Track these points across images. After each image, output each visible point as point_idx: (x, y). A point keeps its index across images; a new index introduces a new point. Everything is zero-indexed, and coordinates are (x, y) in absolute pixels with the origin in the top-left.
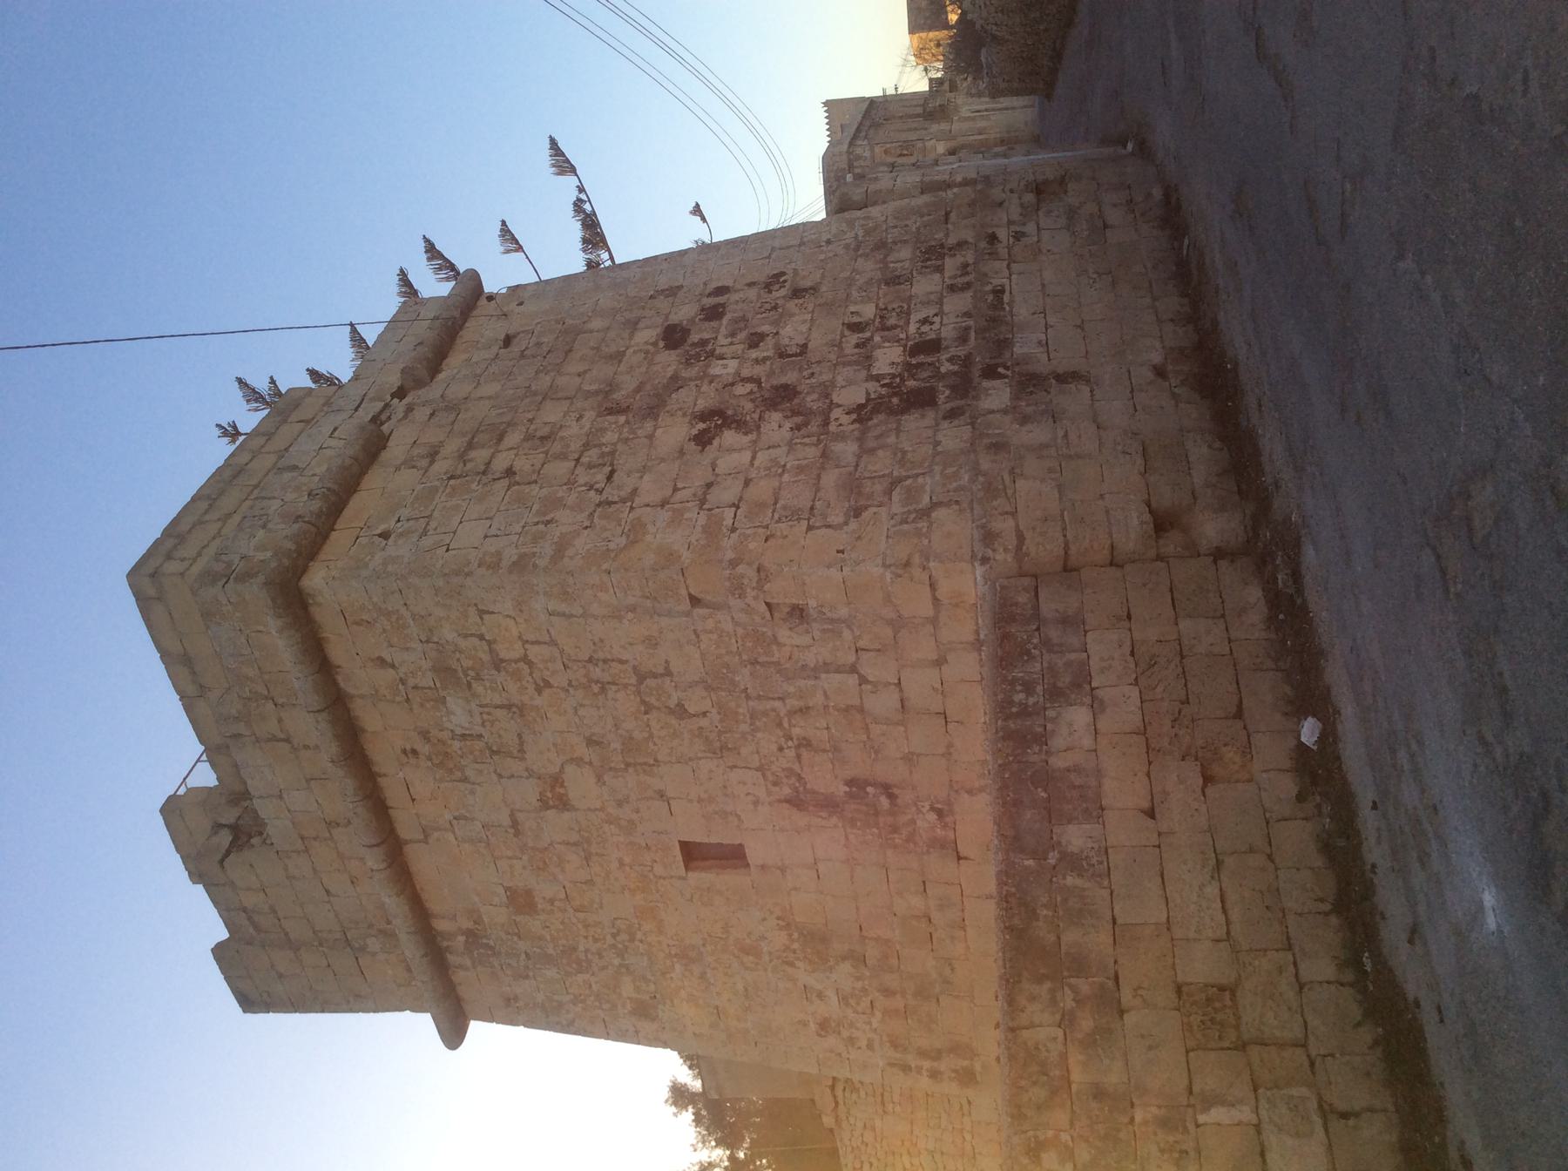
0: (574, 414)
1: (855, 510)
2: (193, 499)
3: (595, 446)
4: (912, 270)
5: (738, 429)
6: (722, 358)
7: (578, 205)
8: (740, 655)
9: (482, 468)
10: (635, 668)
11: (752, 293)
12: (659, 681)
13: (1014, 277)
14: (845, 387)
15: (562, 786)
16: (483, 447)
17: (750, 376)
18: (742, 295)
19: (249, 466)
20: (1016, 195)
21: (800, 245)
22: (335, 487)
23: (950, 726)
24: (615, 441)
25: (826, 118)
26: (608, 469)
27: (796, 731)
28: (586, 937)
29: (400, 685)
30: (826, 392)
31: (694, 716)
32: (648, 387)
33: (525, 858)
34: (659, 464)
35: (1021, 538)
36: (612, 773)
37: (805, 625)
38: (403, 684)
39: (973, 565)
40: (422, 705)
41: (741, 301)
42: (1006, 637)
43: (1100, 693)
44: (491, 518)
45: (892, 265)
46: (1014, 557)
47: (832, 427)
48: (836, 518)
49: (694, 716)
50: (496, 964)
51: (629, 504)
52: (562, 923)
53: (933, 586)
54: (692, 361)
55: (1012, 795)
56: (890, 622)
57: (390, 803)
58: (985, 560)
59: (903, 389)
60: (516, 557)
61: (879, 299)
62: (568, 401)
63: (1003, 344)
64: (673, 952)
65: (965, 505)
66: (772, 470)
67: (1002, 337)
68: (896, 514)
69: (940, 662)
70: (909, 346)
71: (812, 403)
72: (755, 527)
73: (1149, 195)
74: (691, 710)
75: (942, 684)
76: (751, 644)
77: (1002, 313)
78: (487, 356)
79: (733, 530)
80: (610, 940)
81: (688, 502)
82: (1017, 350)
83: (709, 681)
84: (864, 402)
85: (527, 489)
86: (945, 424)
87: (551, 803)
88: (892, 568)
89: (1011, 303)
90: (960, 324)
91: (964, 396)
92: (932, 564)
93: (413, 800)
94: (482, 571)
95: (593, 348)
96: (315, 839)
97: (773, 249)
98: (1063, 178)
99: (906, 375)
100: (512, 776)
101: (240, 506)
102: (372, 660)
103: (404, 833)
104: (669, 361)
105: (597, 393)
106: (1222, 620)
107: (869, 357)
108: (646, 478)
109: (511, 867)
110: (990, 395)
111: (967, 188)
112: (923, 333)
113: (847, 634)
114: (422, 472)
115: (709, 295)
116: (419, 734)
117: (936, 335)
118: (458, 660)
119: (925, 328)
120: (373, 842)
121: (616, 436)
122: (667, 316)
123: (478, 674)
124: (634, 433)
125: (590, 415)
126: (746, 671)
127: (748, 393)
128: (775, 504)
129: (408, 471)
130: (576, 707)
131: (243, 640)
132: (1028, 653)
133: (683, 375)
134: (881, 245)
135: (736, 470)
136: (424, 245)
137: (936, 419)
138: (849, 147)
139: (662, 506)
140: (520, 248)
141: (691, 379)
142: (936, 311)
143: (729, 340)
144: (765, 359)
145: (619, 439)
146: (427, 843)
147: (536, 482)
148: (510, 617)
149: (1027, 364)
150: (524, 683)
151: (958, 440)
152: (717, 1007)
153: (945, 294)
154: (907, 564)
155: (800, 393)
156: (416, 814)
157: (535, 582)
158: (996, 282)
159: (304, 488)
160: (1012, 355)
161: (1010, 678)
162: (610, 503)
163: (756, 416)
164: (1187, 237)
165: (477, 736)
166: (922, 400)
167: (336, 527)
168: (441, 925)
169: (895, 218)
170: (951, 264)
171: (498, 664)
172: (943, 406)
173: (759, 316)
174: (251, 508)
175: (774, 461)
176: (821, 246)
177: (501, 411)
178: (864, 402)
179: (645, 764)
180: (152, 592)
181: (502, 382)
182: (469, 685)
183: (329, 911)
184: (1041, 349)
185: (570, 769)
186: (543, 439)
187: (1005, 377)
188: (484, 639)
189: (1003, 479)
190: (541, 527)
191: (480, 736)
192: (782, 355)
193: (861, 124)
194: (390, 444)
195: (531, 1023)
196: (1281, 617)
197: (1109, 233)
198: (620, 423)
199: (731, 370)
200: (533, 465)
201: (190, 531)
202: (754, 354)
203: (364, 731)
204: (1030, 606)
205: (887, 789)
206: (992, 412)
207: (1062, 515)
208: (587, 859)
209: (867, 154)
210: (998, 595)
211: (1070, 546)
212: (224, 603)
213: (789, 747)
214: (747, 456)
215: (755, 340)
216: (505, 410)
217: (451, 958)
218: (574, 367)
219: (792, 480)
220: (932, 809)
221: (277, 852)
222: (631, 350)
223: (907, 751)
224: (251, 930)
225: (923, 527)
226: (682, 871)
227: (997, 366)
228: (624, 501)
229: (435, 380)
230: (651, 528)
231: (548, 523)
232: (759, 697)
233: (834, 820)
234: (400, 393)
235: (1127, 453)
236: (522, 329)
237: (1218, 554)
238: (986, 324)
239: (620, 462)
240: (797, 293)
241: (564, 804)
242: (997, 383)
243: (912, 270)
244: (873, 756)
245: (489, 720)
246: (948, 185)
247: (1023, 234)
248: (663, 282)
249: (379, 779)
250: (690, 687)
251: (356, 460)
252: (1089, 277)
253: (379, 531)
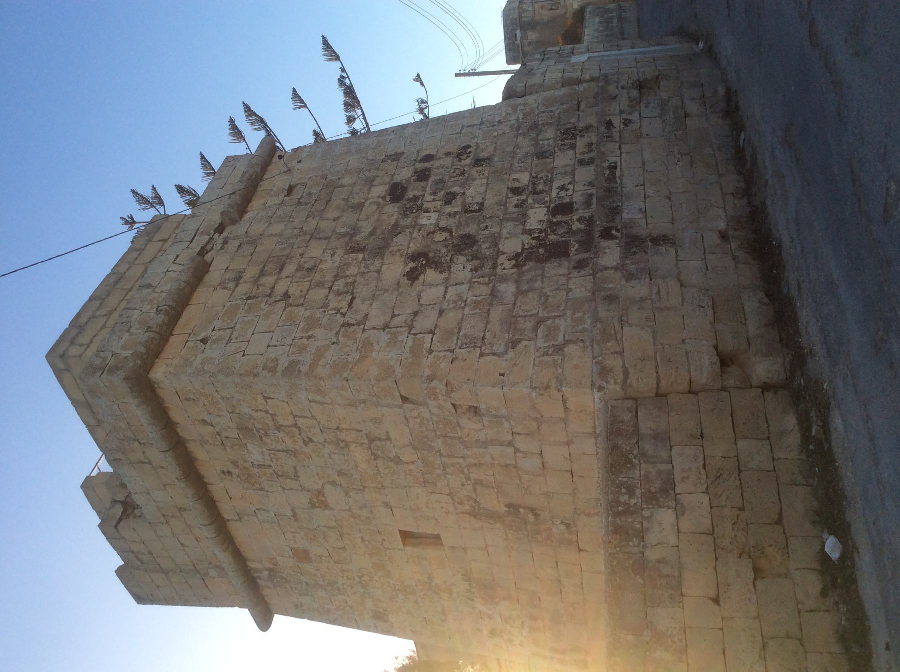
1: (513, 343)
2: (91, 299)
3: (342, 278)
4: (555, 147)
5: (436, 269)
6: (427, 212)
7: (341, 80)
8: (435, 432)
9: (269, 292)
10: (367, 435)
11: (448, 161)
12: (383, 443)
13: (624, 156)
15: (324, 496)
16: (270, 275)
18: (441, 162)
20: (625, 91)
23: (575, 479)
24: (355, 274)
26: (349, 298)
28: (343, 577)
29: (217, 437)
31: (406, 463)
32: (379, 232)
33: (303, 533)
34: (384, 294)
35: (626, 374)
36: (355, 492)
37: (479, 417)
38: (219, 435)
39: (593, 392)
41: (442, 167)
42: (615, 448)
45: (541, 143)
46: (622, 388)
47: (499, 270)
50: (288, 586)
51: (362, 327)
52: (328, 569)
53: (565, 402)
54: (408, 213)
55: (618, 581)
56: (536, 419)
57: (216, 499)
58: (601, 389)
61: (532, 169)
63: (616, 211)
65: (588, 344)
67: (615, 205)
68: (540, 348)
69: (569, 443)
72: (445, 351)
73: (716, 92)
77: (615, 186)
78: (277, 202)
79: (431, 352)
80: (358, 580)
81: (401, 327)
84: (520, 251)
85: (297, 310)
86: (575, 274)
87: (317, 505)
90: (586, 192)
91: (588, 251)
92: (564, 389)
93: (231, 499)
94: (265, 372)
96: (172, 517)
97: (463, 127)
98: (657, 78)
99: (549, 231)
100: (292, 489)
101: (119, 305)
103: (226, 516)
104: (393, 211)
105: (344, 235)
107: (525, 215)
108: (375, 305)
110: (606, 253)
113: (506, 424)
115: (421, 161)
118: (253, 424)
119: (563, 194)
120: (207, 523)
122: (393, 176)
123: (266, 433)
125: (340, 252)
126: (440, 441)
127: (444, 240)
129: (222, 291)
131: (116, 407)
132: (631, 462)
133: (402, 224)
134: (535, 127)
136: (243, 108)
137: (569, 269)
139: (384, 329)
141: (407, 227)
143: (433, 197)
144: (456, 213)
145: (359, 273)
146: (241, 522)
147: (302, 305)
148: (285, 402)
149: (632, 228)
150: (296, 439)
152: (426, 618)
153: (577, 167)
154: (548, 387)
155: (477, 242)
158: (613, 160)
161: (618, 482)
162: (350, 325)
163: (448, 259)
166: (559, 252)
168: (252, 565)
169: (545, 105)
170: (581, 143)
171: (279, 428)
172: (574, 258)
173: (453, 180)
175: (460, 296)
177: (283, 246)
179: (377, 488)
180: (62, 367)
181: (285, 223)
182: (262, 440)
185: (328, 488)
186: (309, 270)
187: (616, 238)
188: (269, 413)
190: (305, 341)
191: (270, 466)
192: (467, 211)
194: (211, 269)
195: (311, 618)
197: (688, 122)
198: (360, 260)
199: (433, 222)
202: (449, 209)
203: (196, 460)
204: (632, 423)
205: (533, 510)
206: (607, 269)
208: (342, 535)
209: (531, 9)
210: (610, 414)
211: (662, 381)
213: (468, 485)
214: (442, 289)
215: (450, 199)
218: (332, 214)
219: (471, 313)
220: (562, 523)
221: (150, 523)
224: (138, 562)
225: (559, 359)
226: (402, 547)
227: (611, 229)
228: (359, 324)
229: (243, 219)
230: (377, 348)
231: (309, 338)
232: (449, 456)
234: (220, 229)
235: (702, 307)
237: (766, 388)
239: (358, 291)
240: (478, 162)
241: (325, 506)
242: (610, 243)
243: (555, 147)
244: (524, 492)
245: (275, 458)
246: (579, 82)
247: (630, 122)
248: (391, 149)
249: (208, 486)
250: (404, 448)
252: (674, 157)
253: (200, 338)
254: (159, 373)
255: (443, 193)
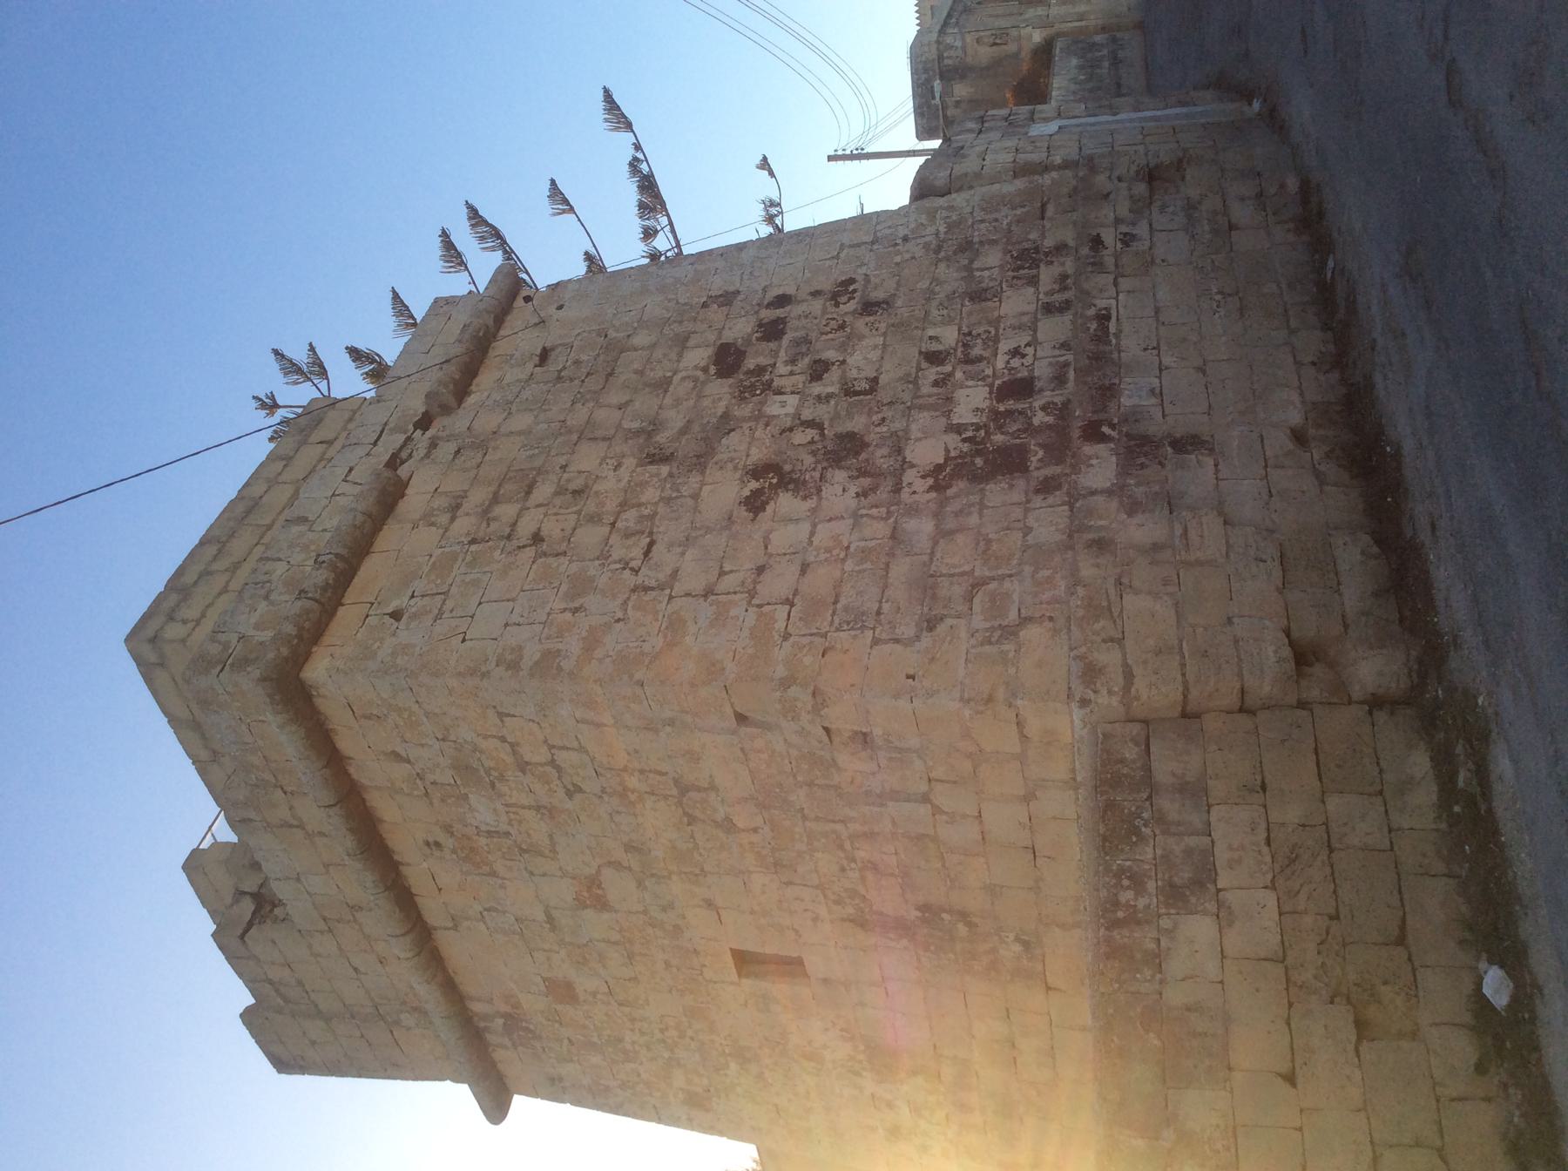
0: (613, 460)
4: (1001, 281)
5: (796, 491)
6: (780, 392)
7: (634, 165)
11: (817, 306)
13: (1121, 297)
14: (920, 439)
15: (599, 887)
17: (811, 418)
19: (264, 499)
20: (1124, 185)
21: (873, 243)
22: (344, 552)
25: (917, 25)
27: (861, 854)
28: (632, 1030)
30: (898, 446)
32: (696, 428)
35: (1129, 676)
36: (654, 880)
37: (869, 751)
38: (421, 779)
40: (443, 801)
41: (805, 316)
42: (1110, 806)
43: (1228, 896)
44: (513, 600)
45: (978, 274)
47: (905, 495)
48: (907, 631)
49: (743, 830)
51: (667, 591)
52: (606, 1014)
54: (746, 394)
56: (970, 756)
58: (1084, 703)
59: (988, 445)
60: (539, 655)
61: (961, 318)
62: (606, 444)
63: (1108, 392)
64: (727, 1051)
66: (834, 553)
67: (1107, 382)
68: (977, 631)
69: (1028, 798)
70: (996, 386)
71: (882, 460)
72: (811, 635)
73: (1282, 186)
74: (740, 825)
75: (1030, 819)
76: (806, 767)
79: (786, 636)
80: (658, 1035)
81: (735, 593)
82: (1126, 401)
83: (760, 799)
84: (942, 461)
86: (1038, 501)
88: (972, 703)
89: (1117, 336)
91: (1060, 461)
93: (440, 890)
95: (636, 372)
98: (1180, 161)
100: (544, 875)
102: (385, 754)
104: (720, 392)
106: (1379, 799)
107: (949, 399)
108: (689, 555)
109: (548, 959)
111: (1067, 171)
112: (1013, 368)
113: (918, 764)
114: (441, 531)
115: (769, 306)
116: (441, 827)
117: (1029, 371)
118: (479, 759)
119: (1016, 362)
120: (398, 932)
121: (658, 494)
124: (678, 491)
125: (630, 462)
127: (809, 443)
128: (835, 603)
130: (611, 814)
132: (1136, 831)
133: (736, 413)
134: (967, 246)
135: (792, 550)
138: (939, 36)
139: (705, 596)
140: (572, 210)
142: (1029, 338)
143: (789, 368)
144: (829, 396)
145: (662, 499)
148: (533, 721)
151: (1053, 528)
154: (990, 699)
156: (444, 903)
157: (560, 689)
158: (1101, 303)
159: (313, 547)
160: (1119, 408)
162: (646, 589)
163: (817, 475)
164: (1331, 256)
165: (505, 833)
166: (1010, 462)
167: (345, 600)
168: (477, 1007)
169: (983, 209)
170: (1047, 275)
171: (523, 766)
172: (1035, 474)
174: (254, 571)
176: (896, 244)
177: (531, 452)
178: (942, 461)
180: (153, 658)
181: (535, 413)
182: (493, 785)
183: (358, 987)
184: (1153, 401)
185: (607, 873)
188: (506, 741)
189: (1107, 592)
190: (568, 615)
191: (507, 834)
193: (952, 9)
194: (409, 491)
195: (578, 1102)
196: (1457, 809)
199: (790, 410)
200: (563, 530)
201: (196, 583)
202: (817, 389)
203: (381, 821)
206: (1093, 493)
207: (1181, 648)
208: (631, 957)
209: (958, 44)
212: (220, 692)
213: (851, 869)
214: (805, 527)
215: (819, 370)
216: (536, 451)
217: (489, 1037)
218: (615, 398)
219: (857, 568)
221: (300, 931)
222: (680, 375)
223: (988, 881)
224: (279, 1000)
226: (735, 977)
227: (1100, 423)
228: (661, 588)
229: (463, 405)
231: (575, 611)
232: (817, 819)
233: (905, 942)
234: (424, 423)
236: (560, 342)
237: (1375, 703)
238: (1087, 361)
240: (869, 307)
241: (602, 904)
242: (1101, 449)
243: (1001, 281)
246: (1045, 168)
247: (1133, 237)
248: (717, 285)
251: (370, 516)
253: (390, 610)
254: (317, 670)
255: (807, 360)
